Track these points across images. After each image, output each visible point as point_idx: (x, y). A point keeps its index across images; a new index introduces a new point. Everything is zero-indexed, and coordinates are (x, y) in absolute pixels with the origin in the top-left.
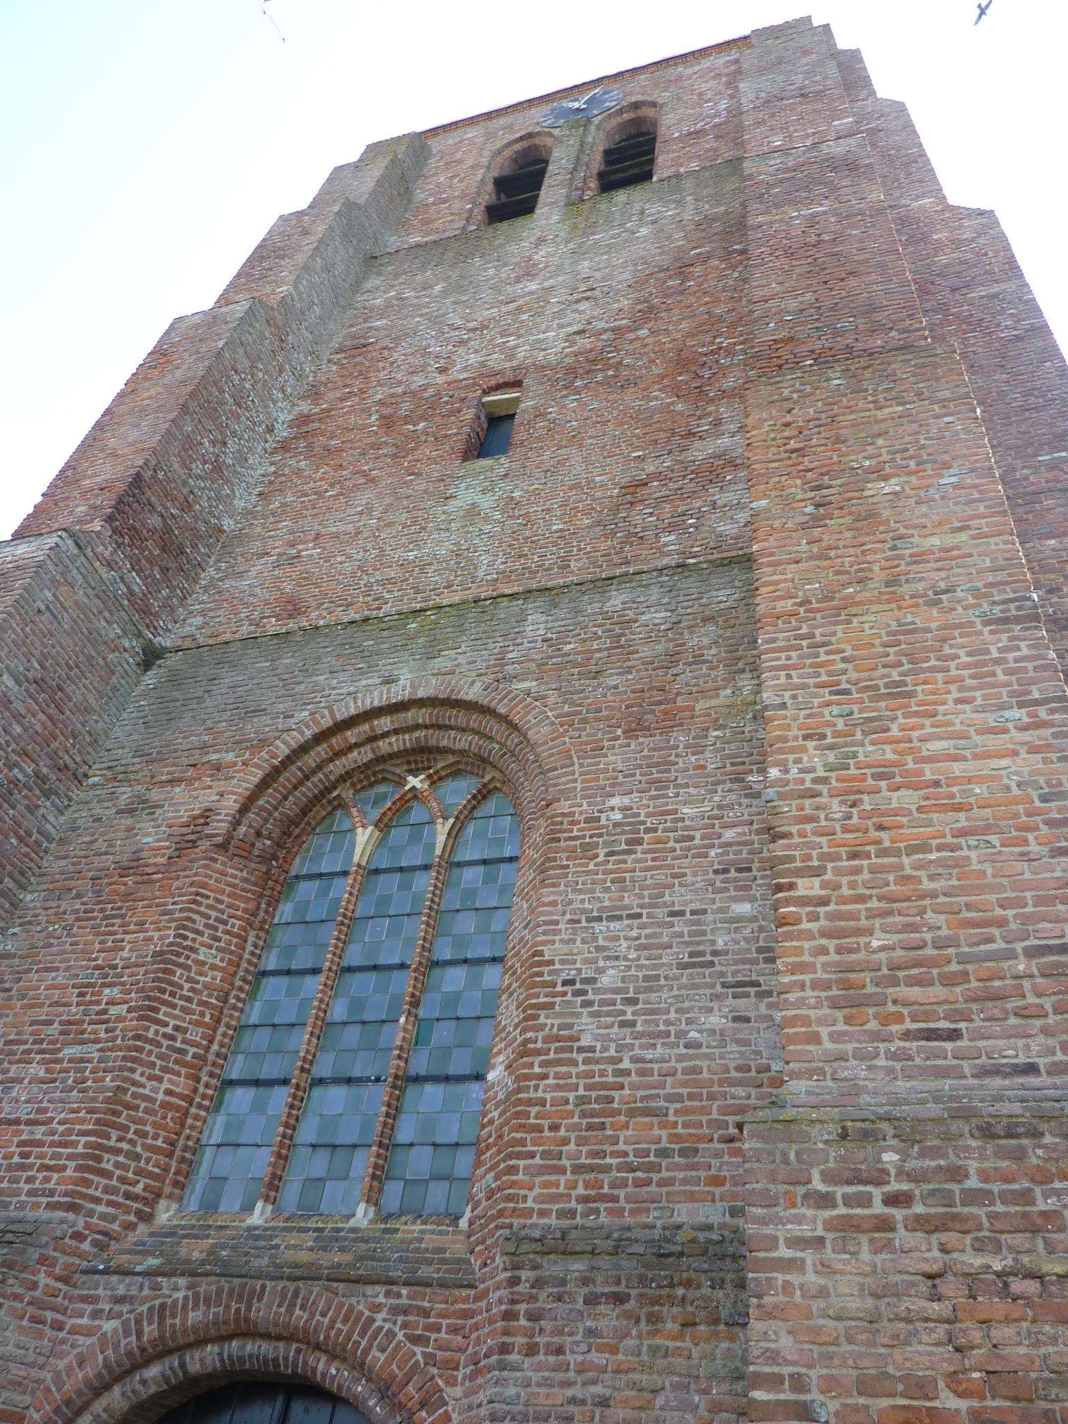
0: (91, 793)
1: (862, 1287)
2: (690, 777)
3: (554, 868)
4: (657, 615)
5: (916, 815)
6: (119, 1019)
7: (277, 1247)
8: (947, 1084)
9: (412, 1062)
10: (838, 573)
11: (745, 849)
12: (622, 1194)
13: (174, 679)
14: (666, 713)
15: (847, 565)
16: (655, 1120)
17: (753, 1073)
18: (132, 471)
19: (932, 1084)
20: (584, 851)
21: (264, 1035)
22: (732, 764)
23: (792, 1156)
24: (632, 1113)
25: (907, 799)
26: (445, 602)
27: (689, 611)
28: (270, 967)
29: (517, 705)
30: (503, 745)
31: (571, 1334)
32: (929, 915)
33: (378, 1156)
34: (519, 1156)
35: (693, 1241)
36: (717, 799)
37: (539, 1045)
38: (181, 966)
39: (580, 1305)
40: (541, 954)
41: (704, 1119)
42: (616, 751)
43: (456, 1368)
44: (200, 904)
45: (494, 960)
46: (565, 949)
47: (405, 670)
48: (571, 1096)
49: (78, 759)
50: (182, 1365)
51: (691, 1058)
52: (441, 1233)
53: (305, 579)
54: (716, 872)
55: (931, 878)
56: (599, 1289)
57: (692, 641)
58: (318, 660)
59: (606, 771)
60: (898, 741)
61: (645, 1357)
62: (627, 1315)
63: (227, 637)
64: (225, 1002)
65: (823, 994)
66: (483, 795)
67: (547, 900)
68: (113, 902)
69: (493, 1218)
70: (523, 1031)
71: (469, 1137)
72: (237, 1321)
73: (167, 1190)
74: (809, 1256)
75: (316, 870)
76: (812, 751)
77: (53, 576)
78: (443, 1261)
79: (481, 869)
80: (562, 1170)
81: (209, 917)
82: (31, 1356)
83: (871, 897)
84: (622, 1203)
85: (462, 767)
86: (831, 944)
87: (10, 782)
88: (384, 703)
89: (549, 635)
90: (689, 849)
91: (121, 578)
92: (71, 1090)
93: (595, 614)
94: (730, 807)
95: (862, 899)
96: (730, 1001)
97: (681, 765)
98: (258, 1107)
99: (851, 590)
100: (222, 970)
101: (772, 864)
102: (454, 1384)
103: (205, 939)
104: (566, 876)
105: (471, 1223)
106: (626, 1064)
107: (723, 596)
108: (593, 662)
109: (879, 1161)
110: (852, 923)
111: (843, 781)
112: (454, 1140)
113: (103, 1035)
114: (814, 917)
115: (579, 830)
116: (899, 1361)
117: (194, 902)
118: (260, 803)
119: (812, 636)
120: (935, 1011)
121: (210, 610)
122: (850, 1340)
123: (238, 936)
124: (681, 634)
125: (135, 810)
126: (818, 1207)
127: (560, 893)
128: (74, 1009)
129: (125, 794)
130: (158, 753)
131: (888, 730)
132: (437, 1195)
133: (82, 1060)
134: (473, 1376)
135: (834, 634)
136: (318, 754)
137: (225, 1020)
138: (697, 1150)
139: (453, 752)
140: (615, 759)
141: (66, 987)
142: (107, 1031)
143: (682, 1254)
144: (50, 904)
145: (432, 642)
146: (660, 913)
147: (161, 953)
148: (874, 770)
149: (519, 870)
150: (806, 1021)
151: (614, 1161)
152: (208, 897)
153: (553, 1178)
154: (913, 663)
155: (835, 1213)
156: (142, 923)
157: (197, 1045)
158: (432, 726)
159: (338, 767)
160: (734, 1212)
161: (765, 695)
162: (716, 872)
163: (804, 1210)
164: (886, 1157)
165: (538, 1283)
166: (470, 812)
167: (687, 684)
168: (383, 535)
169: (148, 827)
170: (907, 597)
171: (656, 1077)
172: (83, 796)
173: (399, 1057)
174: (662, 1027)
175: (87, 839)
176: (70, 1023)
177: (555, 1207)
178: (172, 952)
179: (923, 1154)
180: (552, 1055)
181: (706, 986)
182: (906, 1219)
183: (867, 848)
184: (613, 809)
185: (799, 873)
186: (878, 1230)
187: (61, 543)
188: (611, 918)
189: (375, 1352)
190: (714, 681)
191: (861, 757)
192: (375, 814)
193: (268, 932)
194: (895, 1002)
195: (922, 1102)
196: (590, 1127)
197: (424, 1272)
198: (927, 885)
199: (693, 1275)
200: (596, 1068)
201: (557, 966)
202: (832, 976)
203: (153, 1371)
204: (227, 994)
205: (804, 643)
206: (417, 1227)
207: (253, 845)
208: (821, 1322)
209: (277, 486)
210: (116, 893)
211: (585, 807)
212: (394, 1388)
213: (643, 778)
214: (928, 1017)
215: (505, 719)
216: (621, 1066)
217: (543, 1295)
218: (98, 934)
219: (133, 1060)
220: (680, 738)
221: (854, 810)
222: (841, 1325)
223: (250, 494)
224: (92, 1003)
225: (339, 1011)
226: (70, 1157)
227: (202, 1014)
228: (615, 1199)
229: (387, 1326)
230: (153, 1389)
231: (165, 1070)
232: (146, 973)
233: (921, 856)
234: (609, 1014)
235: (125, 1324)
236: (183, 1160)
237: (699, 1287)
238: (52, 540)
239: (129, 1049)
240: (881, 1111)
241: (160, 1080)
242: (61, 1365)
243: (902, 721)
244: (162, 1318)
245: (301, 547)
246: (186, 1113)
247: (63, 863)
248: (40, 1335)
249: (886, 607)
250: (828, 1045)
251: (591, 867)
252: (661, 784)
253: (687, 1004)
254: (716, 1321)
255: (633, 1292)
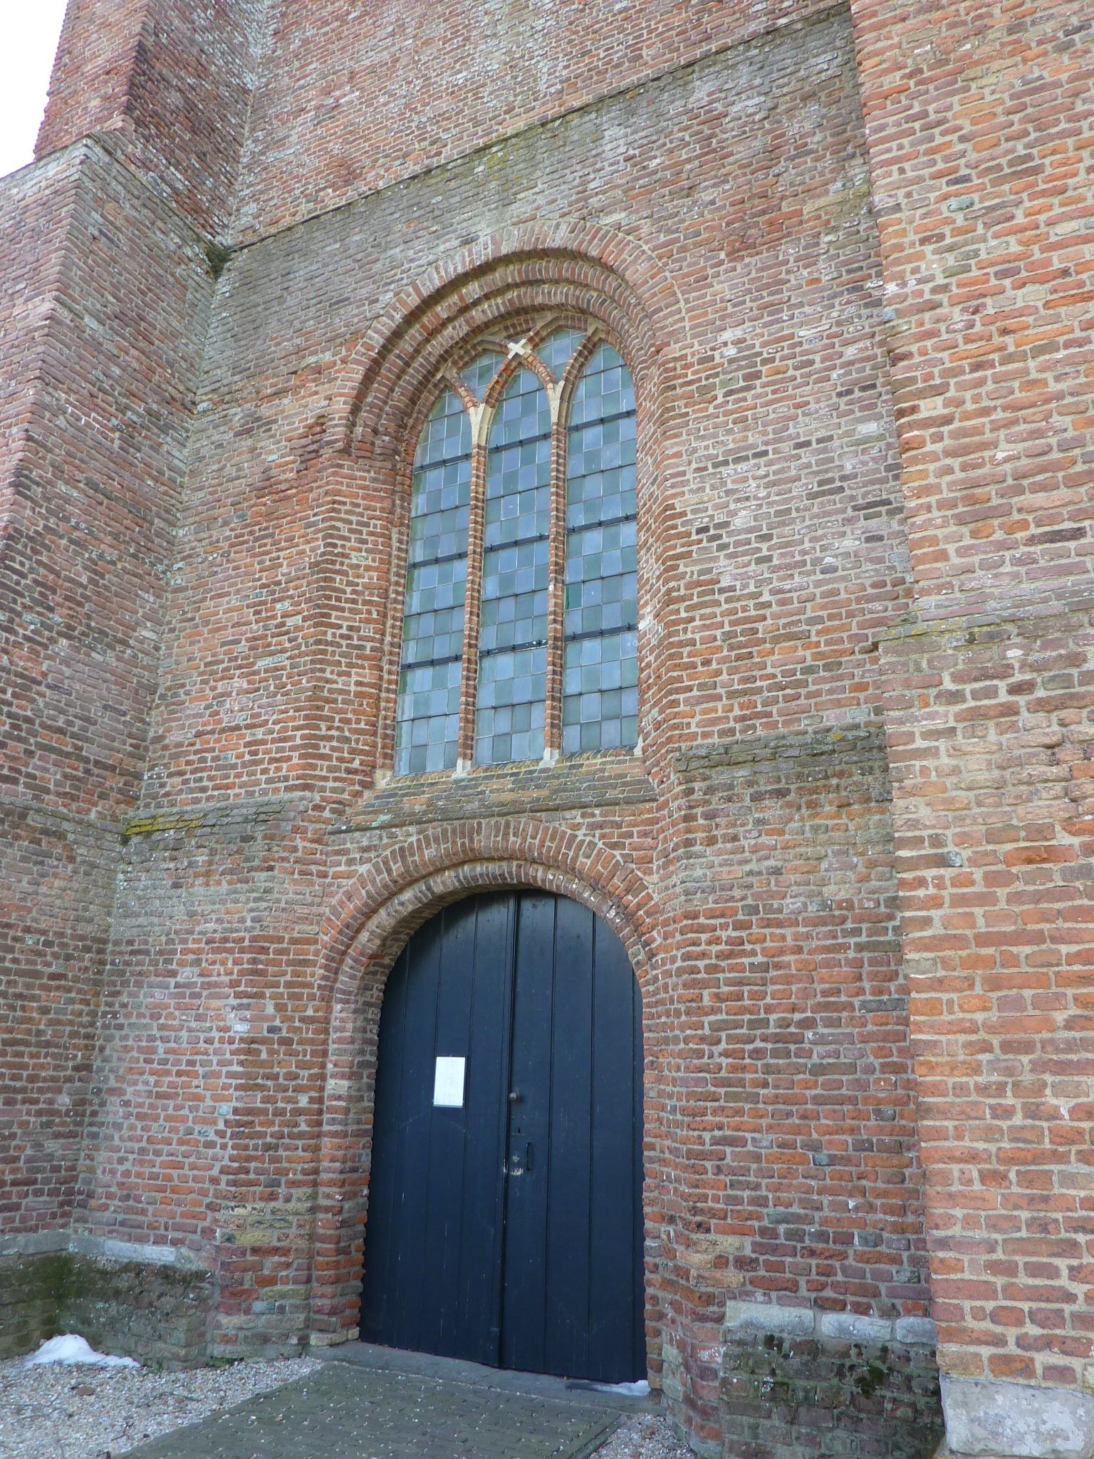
0: (205, 420)
1: (989, 762)
2: (804, 294)
3: (673, 418)
4: (750, 103)
5: (1043, 312)
6: (298, 628)
7: (483, 792)
8: (1069, 581)
9: (567, 623)
10: (952, 26)
11: (868, 365)
12: (774, 709)
13: (248, 282)
14: (771, 224)
15: (962, 12)
16: (799, 643)
17: (889, 588)
18: (133, 42)
19: (1055, 583)
20: (701, 395)
21: (428, 623)
22: (849, 272)
23: (924, 665)
24: (776, 640)
25: (1034, 294)
26: (510, 132)
27: (785, 90)
28: (419, 559)
29: (607, 245)
30: (601, 291)
31: (742, 825)
32: (1055, 417)
33: (553, 708)
34: (678, 691)
35: (843, 739)
36: (835, 314)
37: (682, 592)
38: (338, 572)
39: (747, 802)
40: (672, 507)
41: (845, 635)
42: (722, 278)
43: (651, 862)
44: (339, 511)
45: (627, 518)
46: (695, 498)
47: (483, 225)
48: (718, 633)
49: (182, 388)
50: (429, 888)
51: (828, 582)
52: (619, 762)
53: (352, 134)
54: (840, 395)
55: (1058, 379)
56: (763, 788)
57: (793, 129)
58: (388, 230)
59: (714, 302)
60: (1023, 230)
61: (808, 834)
62: (789, 805)
63: (287, 221)
64: (387, 597)
65: (950, 513)
66: (589, 349)
67: (670, 452)
68: (259, 523)
69: (663, 745)
70: (666, 582)
71: (631, 679)
72: (464, 851)
73: (380, 761)
74: (942, 744)
75: (438, 458)
76: (930, 257)
77: (95, 194)
78: (625, 784)
79: (599, 429)
80: (719, 698)
81: (351, 523)
82: (309, 899)
83: (995, 408)
84: (775, 717)
85: (562, 322)
86: (955, 463)
87: (128, 426)
88: (468, 267)
89: (631, 152)
90: (809, 375)
91: (162, 178)
92: (275, 695)
93: (679, 115)
94: (850, 321)
95: (986, 412)
96: (862, 522)
97: (793, 282)
98: (439, 683)
99: (968, 46)
100: (376, 569)
101: (895, 386)
102: (651, 873)
103: (353, 544)
104: (687, 424)
105: (644, 751)
106: (766, 597)
107: (823, 63)
108: (684, 175)
109: (1005, 658)
110: (976, 439)
111: (965, 285)
112: (617, 685)
113: (287, 645)
114: (938, 438)
115: (694, 373)
116: (1019, 817)
117: (334, 510)
118: (369, 399)
119: (924, 114)
120: (1060, 514)
121: (262, 192)
122: (979, 804)
123: (383, 535)
124: (779, 122)
125: (251, 429)
126: (950, 703)
127: (683, 443)
128: (254, 627)
129: (237, 414)
130: (256, 366)
131: (1012, 217)
132: (611, 732)
133: (276, 669)
134: (665, 866)
135: (950, 108)
136: (413, 337)
137: (390, 613)
138: (840, 664)
139: (550, 308)
140: (721, 288)
141: (241, 608)
142: (290, 641)
143: (833, 751)
144: (203, 535)
145: (506, 185)
146: (786, 447)
147: (317, 564)
148: (997, 268)
149: (638, 424)
150: (934, 540)
151: (764, 684)
152: (344, 503)
153: (711, 705)
154: (1040, 130)
155: (965, 706)
156: (291, 539)
157: (373, 640)
158: (523, 283)
159: (436, 347)
160: (878, 711)
161: (877, 198)
162: (840, 395)
163: (936, 708)
164: (1010, 654)
165: (710, 790)
166: (579, 371)
167: (792, 184)
168: (424, 58)
169: (268, 444)
170: (1033, 45)
171: (796, 605)
172: (197, 424)
173: (555, 621)
174: (798, 558)
175: (215, 467)
176: (255, 639)
177: (716, 729)
178: (326, 561)
179: (1044, 647)
180: (696, 600)
181: (838, 512)
182: (1028, 703)
183: (991, 356)
184: (725, 344)
185: (921, 394)
186: (1003, 715)
187: (89, 153)
188: (737, 460)
189: (581, 859)
190: (822, 174)
191: (983, 255)
192: (483, 390)
193: (408, 526)
194: (1020, 510)
195: (1045, 601)
196: (738, 658)
197: (610, 794)
198: (1054, 387)
199: (844, 766)
200: (738, 605)
201: (690, 517)
202: (958, 494)
203: (407, 895)
204: (387, 591)
205: (917, 125)
206: (599, 760)
207: (373, 444)
208: (954, 793)
209: (290, 18)
210: (259, 514)
211: (696, 347)
212: (602, 882)
213: (754, 305)
214: (1052, 520)
215: (598, 262)
216: (762, 600)
217: (715, 799)
218: (254, 556)
219: (321, 662)
220: (790, 251)
221: (977, 317)
222: (971, 794)
223: (264, 36)
224: (268, 618)
225: (491, 588)
226: (292, 749)
227: (369, 612)
228: (769, 715)
229: (588, 839)
230: (410, 908)
231: (350, 665)
232: (309, 584)
233: (1047, 357)
234: (745, 553)
235: (376, 866)
236: (385, 736)
237: (850, 775)
238: (79, 152)
239: (315, 653)
240: (1005, 614)
241: (348, 674)
242: (334, 901)
243: (1027, 204)
244: (403, 858)
245: (337, 93)
246: (379, 698)
247: (201, 494)
248: (311, 884)
249: (1009, 62)
250: (955, 560)
251: (711, 410)
252: (773, 308)
253: (820, 532)
254: (868, 800)
255: (793, 787)
